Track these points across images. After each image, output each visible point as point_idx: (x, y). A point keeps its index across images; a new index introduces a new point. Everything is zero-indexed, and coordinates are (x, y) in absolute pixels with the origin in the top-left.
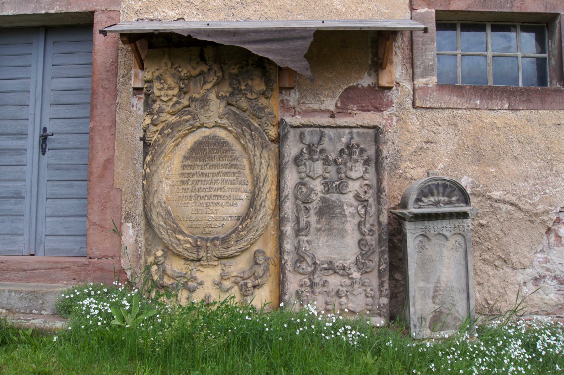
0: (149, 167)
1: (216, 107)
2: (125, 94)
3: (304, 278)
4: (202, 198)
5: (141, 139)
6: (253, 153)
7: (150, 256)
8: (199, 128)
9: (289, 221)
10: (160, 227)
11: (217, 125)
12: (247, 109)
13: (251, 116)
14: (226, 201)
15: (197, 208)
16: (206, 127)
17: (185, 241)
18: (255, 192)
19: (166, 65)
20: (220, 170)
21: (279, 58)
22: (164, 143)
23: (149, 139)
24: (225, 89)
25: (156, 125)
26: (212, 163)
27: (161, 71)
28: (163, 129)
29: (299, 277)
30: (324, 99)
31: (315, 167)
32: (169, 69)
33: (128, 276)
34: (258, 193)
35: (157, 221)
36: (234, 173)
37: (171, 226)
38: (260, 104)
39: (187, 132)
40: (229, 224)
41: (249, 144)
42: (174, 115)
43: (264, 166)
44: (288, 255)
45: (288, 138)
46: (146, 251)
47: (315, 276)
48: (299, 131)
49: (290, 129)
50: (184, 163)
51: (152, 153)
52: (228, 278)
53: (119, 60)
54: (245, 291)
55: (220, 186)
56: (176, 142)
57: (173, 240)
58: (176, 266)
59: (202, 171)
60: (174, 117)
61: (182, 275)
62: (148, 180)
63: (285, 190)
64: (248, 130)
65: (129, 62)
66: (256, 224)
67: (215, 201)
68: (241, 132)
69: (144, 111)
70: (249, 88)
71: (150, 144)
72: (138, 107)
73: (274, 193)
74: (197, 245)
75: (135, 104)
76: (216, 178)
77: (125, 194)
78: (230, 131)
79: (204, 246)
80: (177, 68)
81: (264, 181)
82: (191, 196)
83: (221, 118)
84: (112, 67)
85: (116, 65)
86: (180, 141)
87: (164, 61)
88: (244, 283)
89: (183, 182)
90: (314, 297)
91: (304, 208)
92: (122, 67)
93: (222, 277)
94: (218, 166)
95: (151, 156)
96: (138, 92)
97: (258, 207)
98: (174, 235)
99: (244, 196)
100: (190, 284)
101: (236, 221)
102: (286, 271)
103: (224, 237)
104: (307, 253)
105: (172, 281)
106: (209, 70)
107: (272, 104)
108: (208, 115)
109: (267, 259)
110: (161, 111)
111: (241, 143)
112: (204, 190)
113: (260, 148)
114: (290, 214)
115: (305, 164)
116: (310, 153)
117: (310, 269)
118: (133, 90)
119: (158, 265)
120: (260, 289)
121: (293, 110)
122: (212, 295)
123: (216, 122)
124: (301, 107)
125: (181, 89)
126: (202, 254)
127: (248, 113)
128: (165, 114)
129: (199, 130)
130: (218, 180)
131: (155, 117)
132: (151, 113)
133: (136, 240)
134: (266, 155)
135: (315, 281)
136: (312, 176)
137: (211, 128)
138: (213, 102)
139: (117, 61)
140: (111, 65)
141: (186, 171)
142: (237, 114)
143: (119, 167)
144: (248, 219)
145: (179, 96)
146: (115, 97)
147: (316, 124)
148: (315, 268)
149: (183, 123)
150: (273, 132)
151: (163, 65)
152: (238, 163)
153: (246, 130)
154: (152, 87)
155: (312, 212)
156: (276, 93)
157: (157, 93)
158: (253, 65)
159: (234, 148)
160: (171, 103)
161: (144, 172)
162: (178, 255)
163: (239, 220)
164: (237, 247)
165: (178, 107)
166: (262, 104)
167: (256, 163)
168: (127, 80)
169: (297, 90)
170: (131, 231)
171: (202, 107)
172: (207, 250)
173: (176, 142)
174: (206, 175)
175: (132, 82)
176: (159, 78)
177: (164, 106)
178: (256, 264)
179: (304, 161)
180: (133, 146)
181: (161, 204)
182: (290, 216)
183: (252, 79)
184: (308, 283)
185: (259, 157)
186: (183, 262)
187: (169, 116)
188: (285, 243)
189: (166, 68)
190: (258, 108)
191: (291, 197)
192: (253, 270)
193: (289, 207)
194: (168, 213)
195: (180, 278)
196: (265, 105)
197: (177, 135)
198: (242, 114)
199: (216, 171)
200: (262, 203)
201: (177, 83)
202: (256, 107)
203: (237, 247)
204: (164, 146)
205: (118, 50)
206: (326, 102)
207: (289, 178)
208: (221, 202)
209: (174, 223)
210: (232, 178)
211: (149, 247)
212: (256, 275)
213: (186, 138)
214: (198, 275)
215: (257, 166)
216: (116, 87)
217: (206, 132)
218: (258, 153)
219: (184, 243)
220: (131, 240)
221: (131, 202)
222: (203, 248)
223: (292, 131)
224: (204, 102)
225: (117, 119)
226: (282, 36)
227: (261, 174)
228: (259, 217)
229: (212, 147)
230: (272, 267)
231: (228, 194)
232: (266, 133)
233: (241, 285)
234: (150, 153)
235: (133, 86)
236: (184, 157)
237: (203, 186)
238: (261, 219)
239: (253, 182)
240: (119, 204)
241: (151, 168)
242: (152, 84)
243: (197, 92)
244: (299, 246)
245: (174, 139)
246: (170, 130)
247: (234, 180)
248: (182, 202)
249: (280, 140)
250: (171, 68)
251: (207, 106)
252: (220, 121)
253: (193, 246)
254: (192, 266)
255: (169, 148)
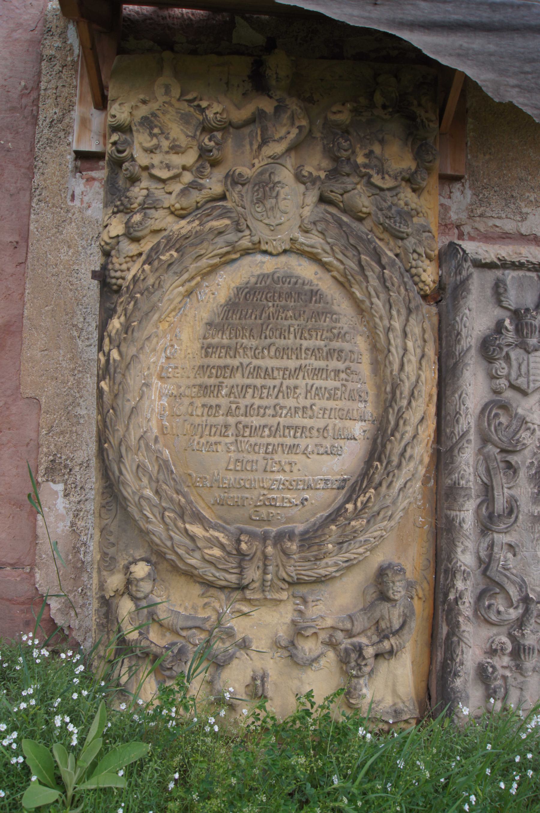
0: (118, 347)
1: (294, 205)
2: (54, 165)
3: (498, 634)
4: (255, 431)
5: (95, 275)
6: (386, 322)
7: (112, 571)
8: (246, 252)
9: (468, 497)
10: (143, 503)
11: (294, 250)
12: (369, 214)
13: (378, 231)
14: (317, 441)
15: (240, 456)
16: (265, 252)
17: (208, 540)
18: (388, 422)
19: (167, 92)
20: (303, 362)
21: (491, 76)
22: (158, 285)
23: (118, 274)
24: (315, 163)
25: (136, 240)
26: (282, 342)
27: (154, 106)
28: (155, 249)
29: (486, 632)
30: (529, 210)
31: (532, 365)
32: (174, 101)
33: (53, 612)
34: (397, 425)
35: (136, 486)
36: (337, 372)
37: (172, 500)
38: (402, 203)
39: (217, 260)
40: (322, 500)
41: (375, 300)
42: (182, 217)
43: (413, 358)
44: (465, 579)
45: (469, 291)
46: (103, 559)
47: (527, 631)
48: (491, 275)
49: (472, 270)
50: (209, 340)
51: (125, 310)
52: (315, 633)
53: (43, 86)
54: (352, 662)
55: (303, 402)
56: (188, 286)
57: (177, 537)
58: (178, 601)
59: (256, 362)
60: (183, 222)
61: (199, 623)
62: (113, 379)
63: (462, 420)
64: (373, 264)
65: (66, 90)
66: (389, 501)
67: (289, 441)
68: (356, 268)
69: (106, 206)
70: (375, 162)
71: (120, 287)
72: (86, 199)
73: (431, 424)
74: (238, 550)
75: (78, 192)
76: (292, 382)
77: (47, 412)
78: (325, 266)
79: (259, 554)
80: (194, 99)
81: (412, 394)
82: (226, 426)
83: (307, 232)
84: (24, 101)
85: (34, 95)
86: (198, 284)
87: (161, 80)
88: (353, 644)
89: (205, 389)
90: (520, 679)
91: (502, 465)
92: (49, 101)
93: (298, 631)
94: (297, 352)
95: (123, 319)
96: (87, 165)
97: (395, 460)
98: (180, 524)
99: (358, 429)
100: (218, 646)
101: (335, 491)
102: (461, 619)
103: (306, 532)
104: (507, 573)
105: (169, 638)
106: (278, 109)
107: (427, 206)
108: (274, 222)
109: (410, 585)
110: (149, 205)
111: (352, 296)
112: (261, 411)
113: (403, 311)
114: (472, 478)
115: (507, 358)
116: (518, 330)
117: (514, 614)
118: (76, 159)
119: (134, 598)
120: (393, 661)
121: (456, 231)
122: (270, 672)
123: (293, 240)
124: (476, 225)
125: (204, 152)
126: (253, 573)
127: (369, 223)
128: (161, 213)
129: (248, 260)
130: (296, 387)
131: (137, 218)
132: (124, 209)
133: (73, 524)
134: (417, 331)
135: (527, 643)
136: (524, 387)
137: (278, 255)
138: (286, 189)
139: (38, 88)
140: (22, 96)
141: (214, 361)
142: (346, 224)
143: (35, 346)
144: (368, 487)
145: (199, 172)
146: (31, 170)
147: (534, 261)
148: (527, 611)
149: (211, 236)
150: (429, 274)
151: (159, 92)
152: (346, 346)
153: (369, 265)
154: (130, 144)
155: (523, 474)
156: (432, 182)
157: (142, 159)
158: (384, 107)
159: (335, 308)
160: (177, 188)
161: (103, 359)
162: (190, 575)
163: (343, 488)
164: (340, 558)
165: (196, 197)
166: (406, 204)
167: (393, 350)
168: (62, 134)
169: (467, 185)
170: (61, 504)
171: (260, 201)
172: (265, 566)
173: (188, 286)
174: (268, 373)
175: (73, 139)
176: (148, 123)
177: (158, 191)
178: (387, 599)
179: (506, 349)
180: (71, 294)
181: (147, 445)
182: (471, 484)
183: (382, 142)
184: (509, 647)
185: (399, 333)
186: (197, 590)
187: (170, 219)
188: (459, 550)
189: (166, 99)
190: (400, 213)
191: (472, 436)
192: (377, 615)
193: (468, 462)
194: (164, 465)
195: (190, 632)
196: (413, 206)
197: (193, 268)
198: (355, 225)
199: (292, 364)
200: (405, 450)
201: (194, 137)
202: (394, 209)
203: (340, 558)
204: (158, 294)
205: (42, 60)
206: (530, 217)
207: (470, 390)
208: (303, 442)
209: (178, 492)
210: (331, 384)
211: (112, 551)
212: (383, 625)
213: (212, 277)
214: (240, 626)
215: (395, 358)
216: (32, 149)
217: (267, 265)
218: (397, 325)
219: (206, 546)
220: (61, 525)
221: (62, 433)
222: (255, 560)
223: (476, 274)
224: (264, 187)
225: (32, 227)
226: (497, 17)
227: (403, 376)
228: (398, 485)
229: (283, 303)
230: (417, 604)
231: (320, 423)
232: (412, 276)
233: (346, 650)
234: (119, 309)
235: (75, 147)
236: (210, 324)
237: (257, 402)
238: (401, 490)
239: (378, 396)
240: (33, 435)
241: (123, 349)
242: (128, 137)
243: (245, 162)
244: (490, 556)
245: (186, 276)
246: (175, 254)
247: (336, 389)
248: (203, 440)
249: (445, 298)
250: (179, 100)
251: (271, 197)
252: (302, 240)
253: (229, 553)
254: (219, 602)
255: (171, 301)
